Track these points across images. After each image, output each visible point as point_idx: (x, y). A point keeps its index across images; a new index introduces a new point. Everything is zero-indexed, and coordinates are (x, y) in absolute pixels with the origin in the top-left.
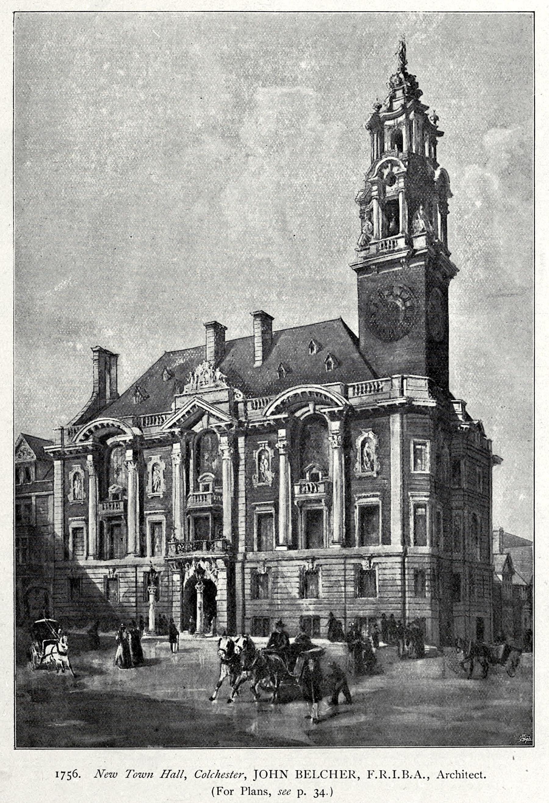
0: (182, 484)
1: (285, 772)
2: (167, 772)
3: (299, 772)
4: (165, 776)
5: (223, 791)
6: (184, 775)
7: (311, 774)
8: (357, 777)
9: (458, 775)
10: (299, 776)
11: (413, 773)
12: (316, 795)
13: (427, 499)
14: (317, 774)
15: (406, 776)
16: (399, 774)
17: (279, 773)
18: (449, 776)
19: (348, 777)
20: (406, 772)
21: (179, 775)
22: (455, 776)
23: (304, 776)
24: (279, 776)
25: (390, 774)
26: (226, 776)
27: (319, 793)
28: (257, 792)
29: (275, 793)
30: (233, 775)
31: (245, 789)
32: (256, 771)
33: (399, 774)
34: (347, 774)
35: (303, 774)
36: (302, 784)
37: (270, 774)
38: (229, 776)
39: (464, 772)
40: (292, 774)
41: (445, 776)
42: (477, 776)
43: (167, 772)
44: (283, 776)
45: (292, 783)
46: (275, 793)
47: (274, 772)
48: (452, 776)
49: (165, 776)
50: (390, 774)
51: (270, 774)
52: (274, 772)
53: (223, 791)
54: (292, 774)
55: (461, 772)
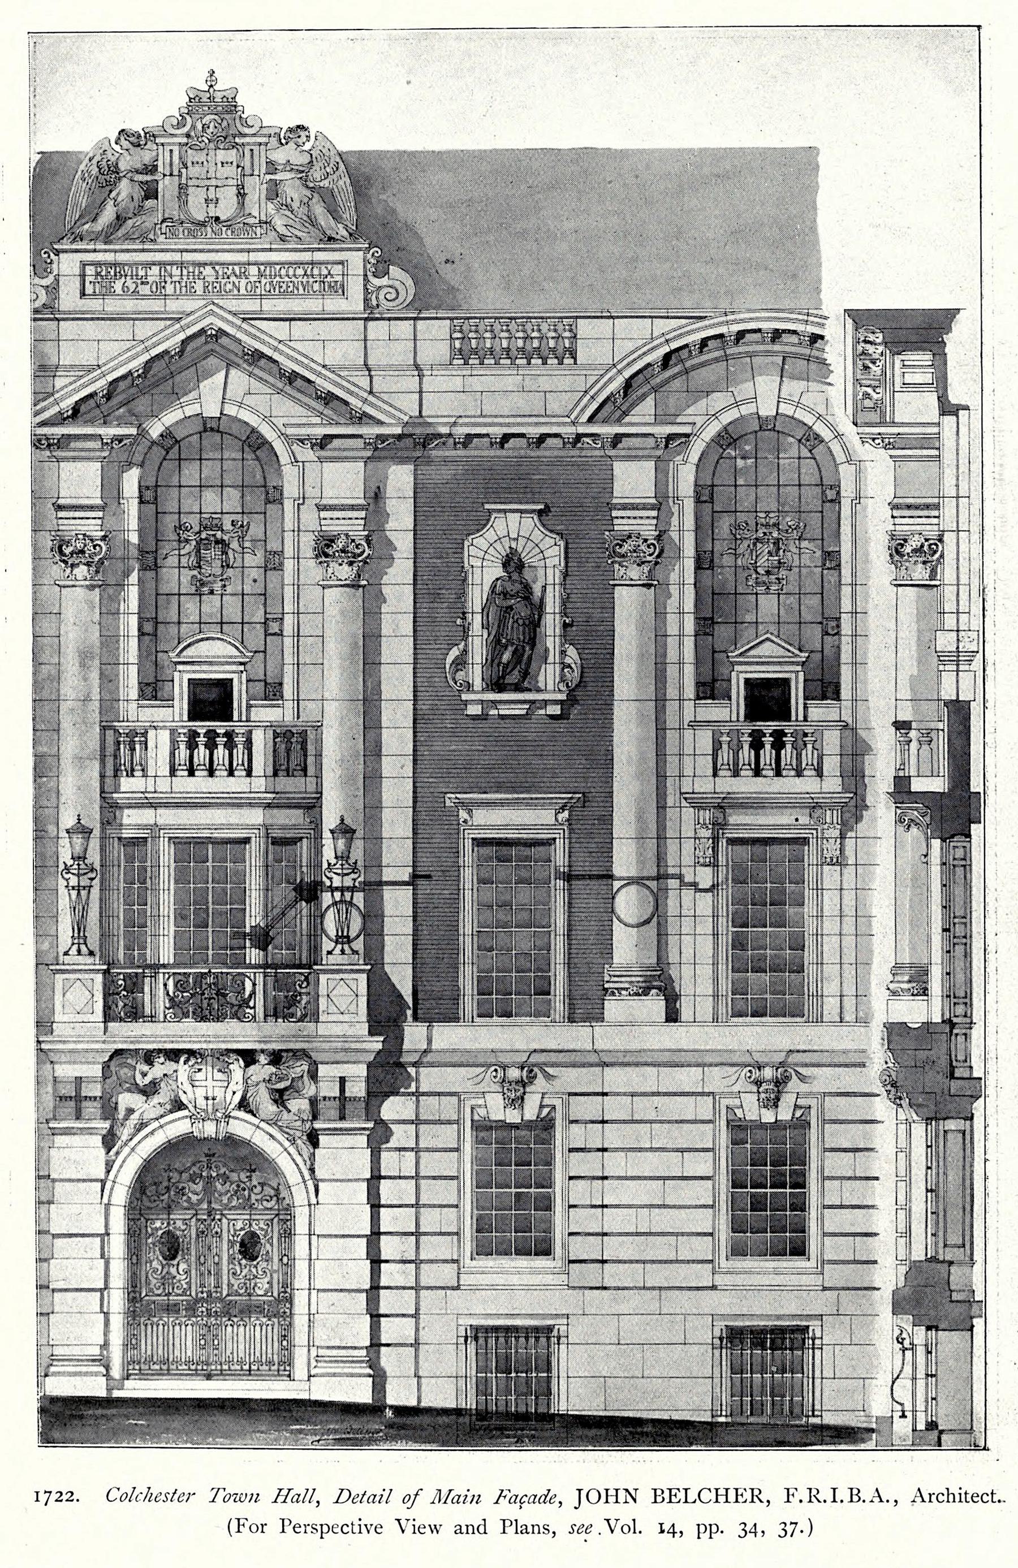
0: (527, 804)
1: (633, 1493)
2: (284, 1492)
3: (659, 1492)
4: (281, 1499)
5: (247, 1525)
6: (315, 1499)
7: (681, 1495)
8: (764, 1500)
9: (951, 1497)
10: (659, 1499)
11: (867, 1494)
12: (743, 1534)
13: (256, 817)
14: (692, 1496)
15: (855, 1498)
16: (843, 1494)
17: (622, 1494)
18: (934, 1498)
19: (806, 1498)
20: (855, 1492)
21: (384, 1499)
22: (945, 1498)
23: (667, 1500)
24: (621, 1499)
25: (826, 1494)
26: (163, 1497)
27: (748, 1529)
28: (464, 1530)
29: (563, 1530)
30: (176, 1497)
31: (508, 1523)
32: (580, 1490)
33: (843, 1494)
34: (748, 1495)
35: (666, 1495)
36: (667, 1513)
37: (605, 1496)
38: (169, 1497)
39: (963, 1492)
40: (645, 1496)
41: (926, 1498)
42: (985, 1498)
43: (284, 1492)
44: (629, 1499)
45: (648, 1514)
46: (563, 1530)
47: (612, 1492)
48: (941, 1498)
49: (281, 1499)
50: (826, 1494)
51: (605, 1496)
52: (612, 1492)
53: (247, 1525)
54: (645, 1496)
55: (956, 1492)
